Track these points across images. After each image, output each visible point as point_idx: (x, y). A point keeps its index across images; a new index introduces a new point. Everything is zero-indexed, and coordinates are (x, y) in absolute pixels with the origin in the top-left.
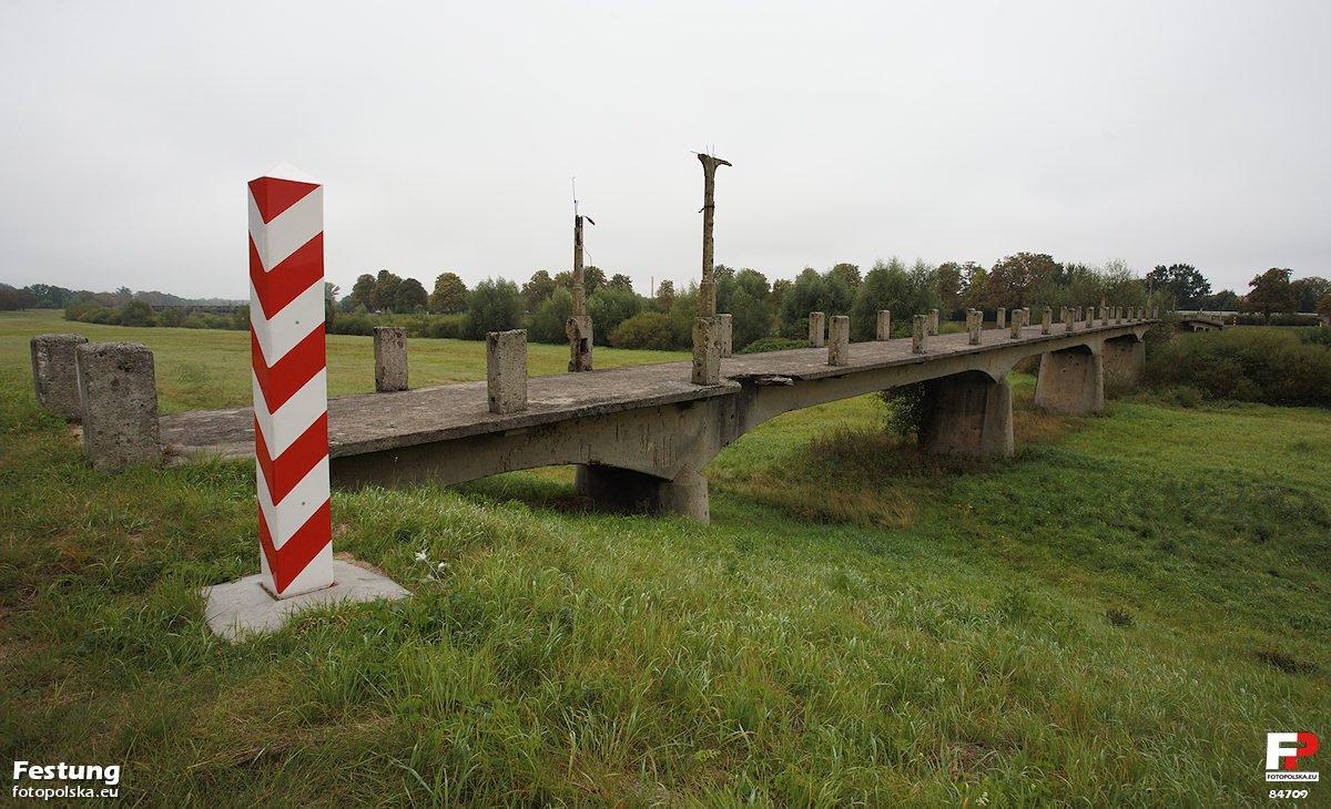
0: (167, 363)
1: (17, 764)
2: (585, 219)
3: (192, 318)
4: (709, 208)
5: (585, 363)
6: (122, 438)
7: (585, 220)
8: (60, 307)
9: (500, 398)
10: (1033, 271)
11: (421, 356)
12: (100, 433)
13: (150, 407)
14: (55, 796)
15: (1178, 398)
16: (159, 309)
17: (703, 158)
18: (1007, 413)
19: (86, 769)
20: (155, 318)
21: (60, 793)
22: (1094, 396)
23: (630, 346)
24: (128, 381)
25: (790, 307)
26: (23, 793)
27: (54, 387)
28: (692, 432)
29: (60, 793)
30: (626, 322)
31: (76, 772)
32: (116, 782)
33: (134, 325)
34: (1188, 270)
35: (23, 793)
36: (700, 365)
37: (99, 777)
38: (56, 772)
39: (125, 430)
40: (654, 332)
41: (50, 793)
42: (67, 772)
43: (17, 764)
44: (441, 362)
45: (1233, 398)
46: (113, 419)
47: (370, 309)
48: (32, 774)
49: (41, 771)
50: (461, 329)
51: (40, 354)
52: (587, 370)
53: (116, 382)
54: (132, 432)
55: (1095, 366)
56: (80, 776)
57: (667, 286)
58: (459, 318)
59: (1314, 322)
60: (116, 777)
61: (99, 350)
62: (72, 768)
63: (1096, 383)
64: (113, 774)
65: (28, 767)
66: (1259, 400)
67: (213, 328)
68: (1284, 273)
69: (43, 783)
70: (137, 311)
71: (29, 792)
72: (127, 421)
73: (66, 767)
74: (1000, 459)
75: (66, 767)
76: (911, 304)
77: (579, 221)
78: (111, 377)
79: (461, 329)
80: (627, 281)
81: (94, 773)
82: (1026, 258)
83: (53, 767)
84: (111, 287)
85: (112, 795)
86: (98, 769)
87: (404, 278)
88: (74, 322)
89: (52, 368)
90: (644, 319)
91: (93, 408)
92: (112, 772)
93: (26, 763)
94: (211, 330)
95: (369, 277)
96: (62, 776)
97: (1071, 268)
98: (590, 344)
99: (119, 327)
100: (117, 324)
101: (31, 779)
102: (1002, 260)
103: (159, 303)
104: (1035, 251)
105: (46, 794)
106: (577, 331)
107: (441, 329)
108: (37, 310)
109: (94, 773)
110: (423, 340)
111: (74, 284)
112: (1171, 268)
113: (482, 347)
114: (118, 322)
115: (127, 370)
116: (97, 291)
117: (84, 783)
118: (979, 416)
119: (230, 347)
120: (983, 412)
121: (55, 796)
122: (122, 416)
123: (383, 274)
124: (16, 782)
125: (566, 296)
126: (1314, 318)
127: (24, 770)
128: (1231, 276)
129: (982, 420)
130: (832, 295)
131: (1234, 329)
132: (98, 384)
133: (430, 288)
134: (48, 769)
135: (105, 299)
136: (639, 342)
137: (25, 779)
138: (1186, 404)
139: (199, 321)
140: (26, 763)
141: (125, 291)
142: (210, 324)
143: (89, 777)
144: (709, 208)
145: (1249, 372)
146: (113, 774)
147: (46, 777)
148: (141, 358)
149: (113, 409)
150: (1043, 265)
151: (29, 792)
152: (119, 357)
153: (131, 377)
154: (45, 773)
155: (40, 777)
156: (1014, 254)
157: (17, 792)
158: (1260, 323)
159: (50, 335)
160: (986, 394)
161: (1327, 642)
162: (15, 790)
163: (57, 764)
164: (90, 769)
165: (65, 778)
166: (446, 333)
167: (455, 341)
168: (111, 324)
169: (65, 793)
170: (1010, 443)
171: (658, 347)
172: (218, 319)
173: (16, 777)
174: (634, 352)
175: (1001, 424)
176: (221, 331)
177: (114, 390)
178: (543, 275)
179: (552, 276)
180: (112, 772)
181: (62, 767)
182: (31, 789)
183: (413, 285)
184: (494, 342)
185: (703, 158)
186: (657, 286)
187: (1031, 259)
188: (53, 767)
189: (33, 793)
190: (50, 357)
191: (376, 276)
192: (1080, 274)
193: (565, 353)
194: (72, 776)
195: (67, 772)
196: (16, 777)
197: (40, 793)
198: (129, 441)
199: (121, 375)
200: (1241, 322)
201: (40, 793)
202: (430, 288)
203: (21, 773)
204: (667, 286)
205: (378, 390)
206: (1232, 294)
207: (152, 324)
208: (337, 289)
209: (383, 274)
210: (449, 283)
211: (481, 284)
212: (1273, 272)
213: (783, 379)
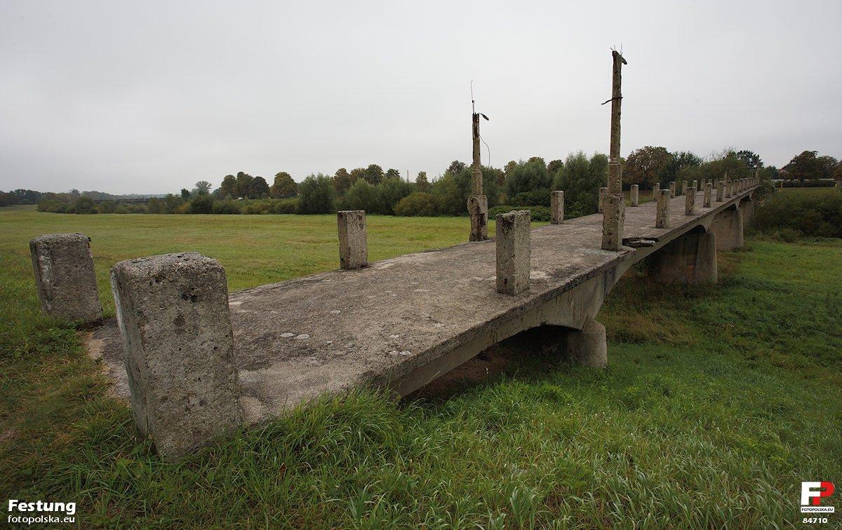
0: (109, 237)
1: (11, 502)
2: (481, 116)
3: (119, 207)
4: (617, 99)
5: (483, 234)
6: (194, 401)
7: (481, 117)
8: (35, 203)
9: (513, 279)
10: (654, 158)
11: (275, 226)
12: (164, 399)
13: (225, 349)
14: (35, 518)
15: (782, 236)
16: (98, 202)
17: (615, 54)
18: (714, 254)
19: (54, 510)
20: (96, 209)
21: (38, 520)
22: (738, 237)
23: (408, 214)
24: (195, 315)
25: (511, 186)
26: (15, 520)
27: (60, 291)
28: (591, 290)
29: (38, 520)
30: (405, 199)
31: (48, 507)
32: (73, 513)
33: (83, 213)
34: (749, 154)
35: (15, 520)
36: (610, 234)
37: (63, 510)
38: (35, 506)
39: (197, 388)
40: (423, 204)
41: (31, 520)
42: (42, 507)
43: (11, 502)
44: (289, 230)
45: (818, 235)
46: (180, 377)
47: (235, 197)
48: (20, 508)
49: (26, 506)
50: (296, 207)
51: (42, 258)
52: (485, 239)
53: (179, 321)
54: (204, 389)
55: (738, 218)
56: (51, 509)
57: (422, 176)
58: (294, 201)
59: (831, 184)
60: (74, 509)
61: (154, 272)
62: (46, 504)
63: (738, 228)
64: (71, 508)
65: (18, 504)
66: (834, 235)
67: (135, 213)
68: (812, 154)
69: (27, 514)
70: (85, 204)
71: (18, 519)
72: (197, 375)
73: (42, 504)
74: (709, 285)
75: (42, 504)
76: (592, 181)
77: (476, 117)
78: (173, 312)
79: (296, 207)
80: (397, 173)
81: (60, 507)
82: (649, 149)
83: (34, 504)
84: (66, 189)
85: (71, 521)
86: (62, 505)
87: (254, 176)
88: (44, 213)
89: (55, 272)
90: (416, 197)
91: (151, 364)
92: (71, 507)
93: (17, 501)
94: (133, 214)
95: (231, 176)
96: (39, 509)
97: (683, 155)
98: (486, 218)
99: (74, 214)
100: (73, 213)
101: (19, 511)
102: (635, 152)
103: (98, 198)
104: (655, 145)
105: (29, 521)
106: (478, 208)
107: (283, 208)
108: (20, 206)
109: (60, 507)
110: (272, 215)
111: (42, 189)
112: (739, 153)
113: (332, 219)
114: (72, 212)
115: (194, 299)
116: (57, 192)
117: (53, 514)
118: (692, 257)
119: (148, 225)
120: (696, 253)
121: (35, 518)
122: (190, 369)
123: (241, 174)
124: (10, 513)
125: (364, 184)
126: (830, 182)
127: (15, 505)
128: (777, 157)
129: (695, 259)
130: (539, 177)
131: (781, 190)
132: (157, 327)
133: (271, 182)
134: (30, 505)
135: (62, 197)
136: (413, 212)
137: (16, 512)
138: (788, 240)
139: (125, 209)
140: (17, 501)
141: (75, 192)
142: (132, 211)
143: (57, 510)
144: (617, 99)
145: (826, 219)
146: (71, 508)
147: (29, 510)
148: (211, 279)
149: (178, 360)
150: (660, 153)
151: (18, 519)
152: (183, 281)
153: (200, 309)
154: (28, 508)
155: (25, 510)
156: (642, 147)
157: (11, 519)
158: (797, 186)
159: (51, 236)
160: (698, 240)
161: (841, 387)
162: (9, 518)
163: (36, 502)
164: (57, 505)
165: (41, 510)
166: (287, 210)
167: (293, 215)
168: (68, 213)
169: (41, 520)
170: (715, 275)
171: (426, 215)
172: (137, 207)
173: (10, 510)
174: (411, 218)
175: (709, 261)
176: (140, 215)
177: (179, 332)
178: (343, 171)
179: (349, 172)
180: (71, 507)
181: (39, 503)
182: (19, 518)
183: (260, 181)
184: (340, 216)
185: (615, 54)
186: (416, 176)
187: (653, 150)
188: (34, 504)
189: (21, 520)
190: (53, 260)
191: (236, 176)
192: (689, 160)
193: (466, 223)
194: (46, 509)
195: (42, 507)
196: (10, 510)
197: (25, 520)
198: (202, 403)
199: (187, 307)
200: (785, 185)
201: (25, 520)
202: (271, 182)
203: (13, 507)
204: (422, 176)
205: (342, 268)
206: (774, 168)
207: (95, 212)
208: (210, 185)
209: (241, 174)
210: (283, 179)
211: (307, 178)
212: (806, 153)
213: (648, 242)
